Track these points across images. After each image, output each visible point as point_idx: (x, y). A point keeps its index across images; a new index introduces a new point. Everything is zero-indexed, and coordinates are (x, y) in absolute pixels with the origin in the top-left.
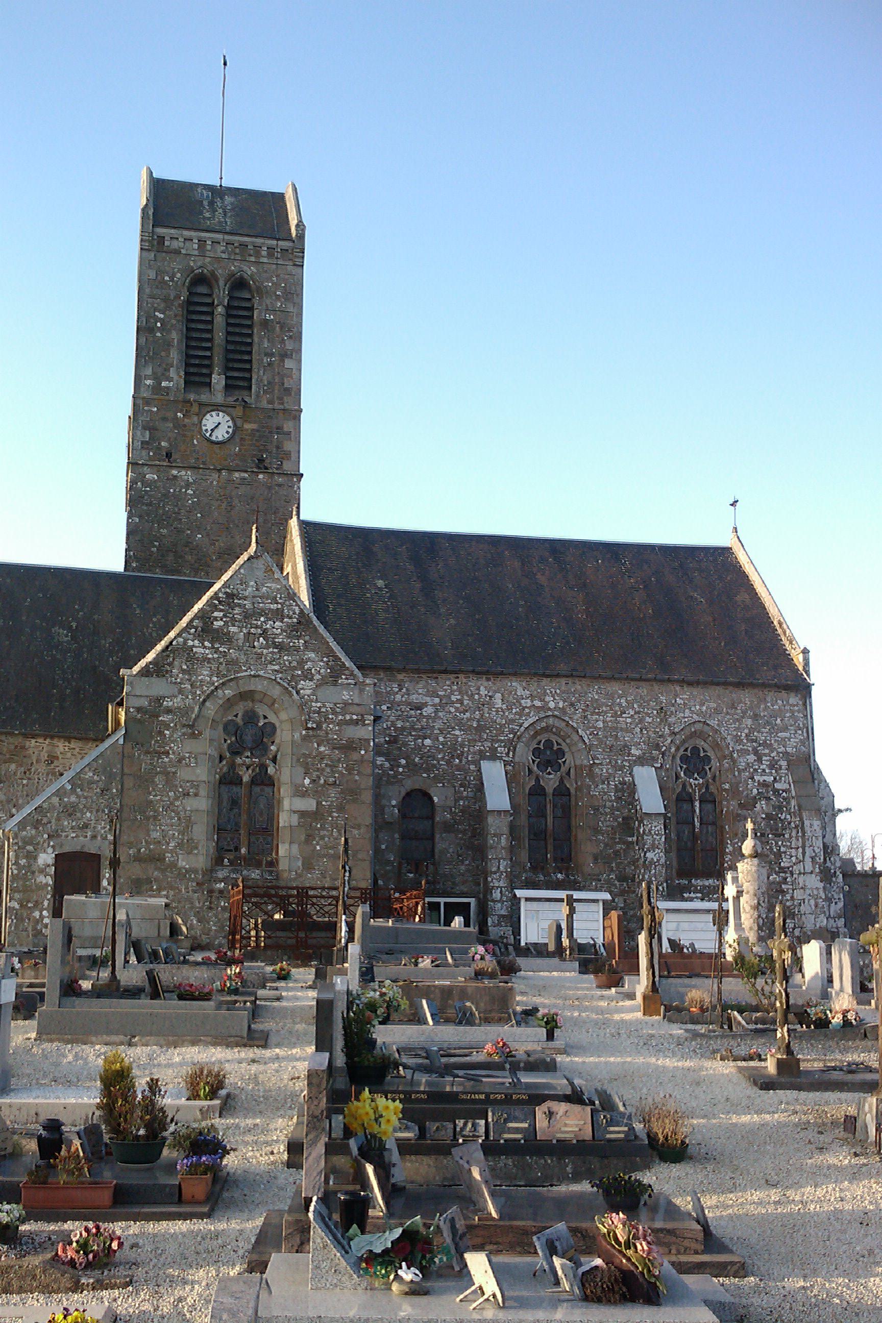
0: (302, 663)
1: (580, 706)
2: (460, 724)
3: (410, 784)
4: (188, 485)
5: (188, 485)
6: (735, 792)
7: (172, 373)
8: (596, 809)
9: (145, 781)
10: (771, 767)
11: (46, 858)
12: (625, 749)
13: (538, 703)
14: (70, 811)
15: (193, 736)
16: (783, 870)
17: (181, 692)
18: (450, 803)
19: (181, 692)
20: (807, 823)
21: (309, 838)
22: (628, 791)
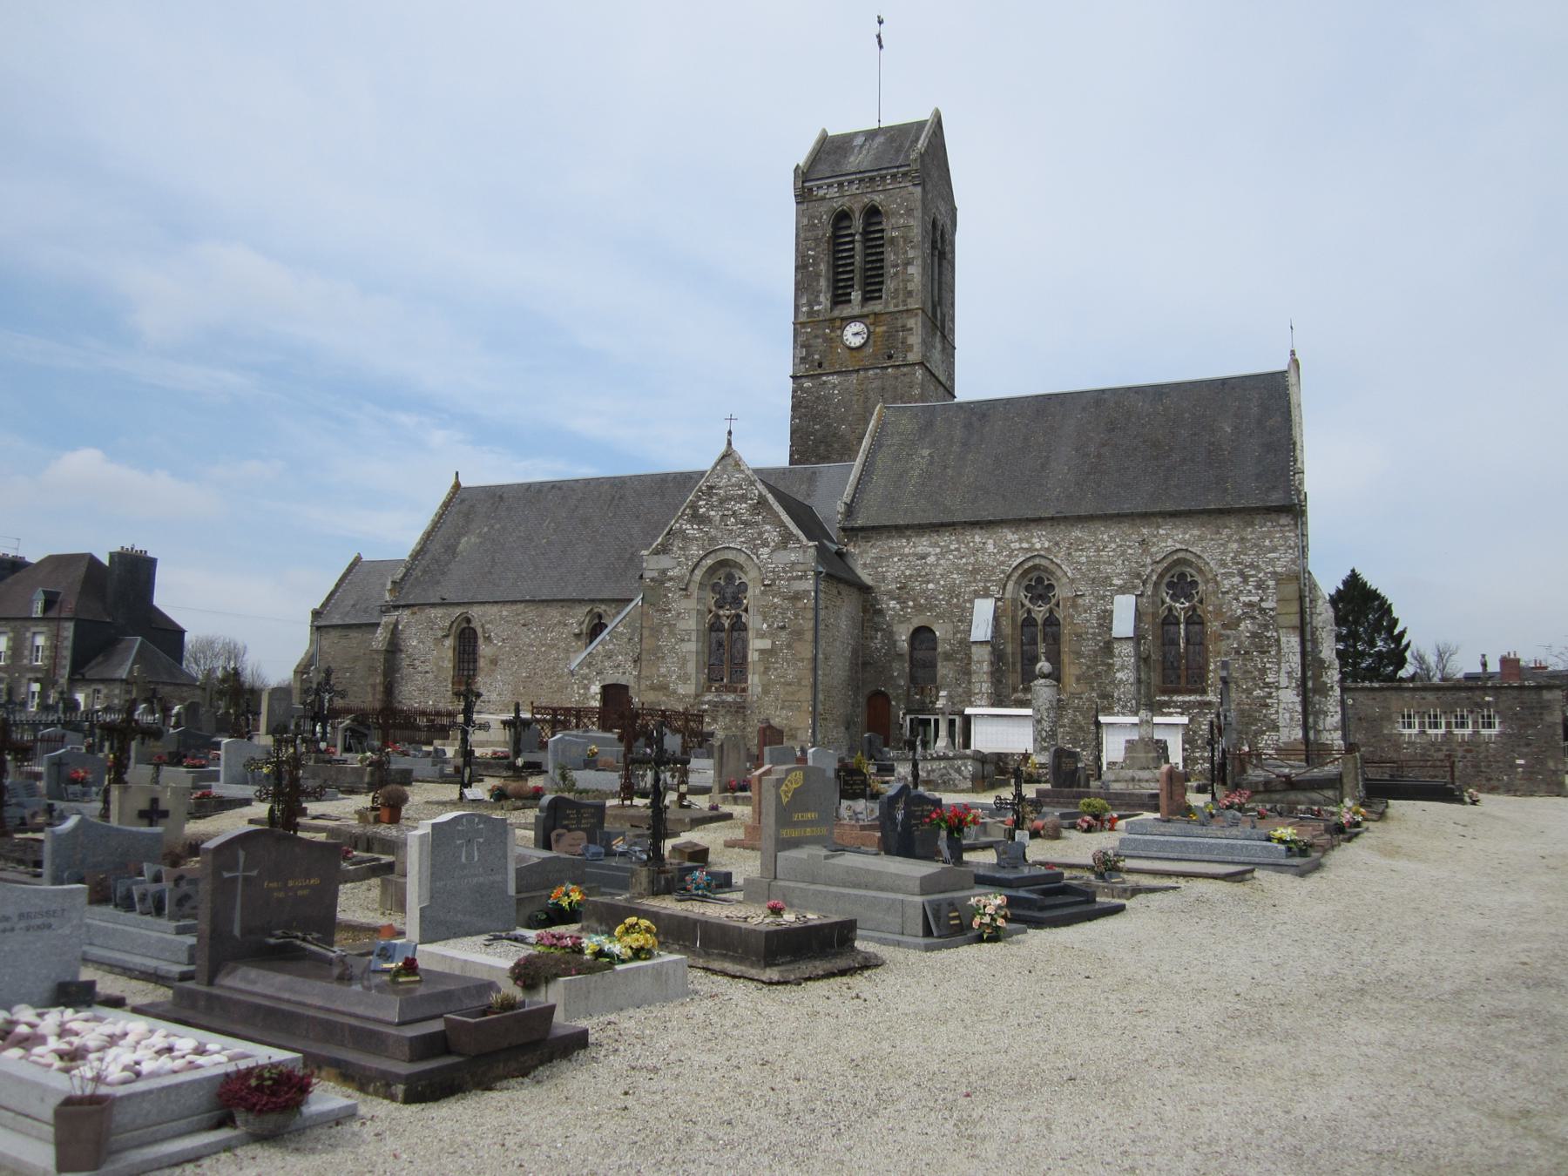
0: (761, 534)
1: (1065, 545)
2: (958, 568)
3: (917, 622)
4: (834, 387)
5: (834, 387)
6: (1218, 613)
7: (822, 298)
8: (1079, 635)
9: (656, 632)
10: (1258, 587)
11: (596, 689)
12: (1107, 580)
13: (1025, 545)
14: (609, 656)
15: (687, 596)
16: (1267, 685)
17: (679, 564)
18: (950, 636)
19: (679, 564)
20: (1283, 639)
21: (767, 669)
22: (1106, 618)
